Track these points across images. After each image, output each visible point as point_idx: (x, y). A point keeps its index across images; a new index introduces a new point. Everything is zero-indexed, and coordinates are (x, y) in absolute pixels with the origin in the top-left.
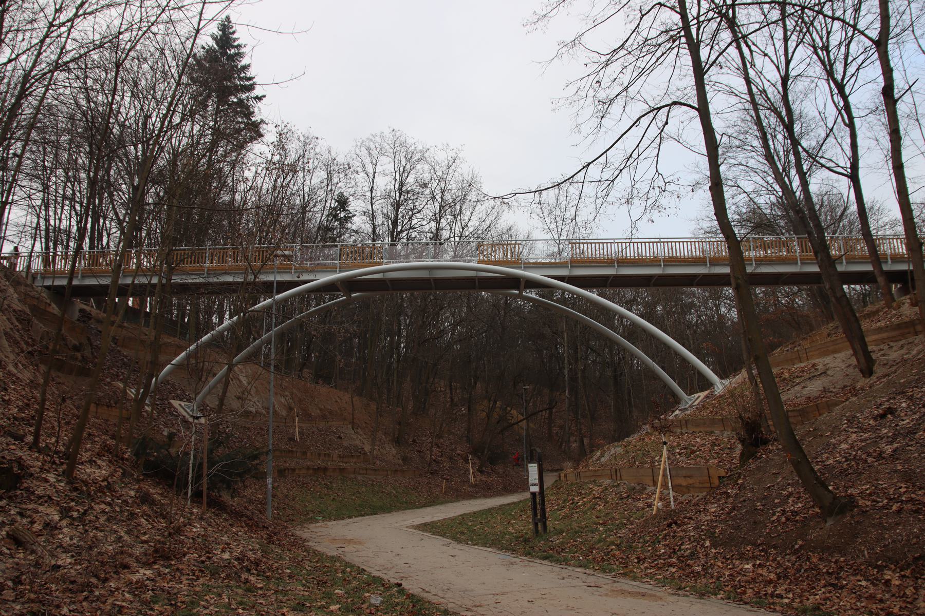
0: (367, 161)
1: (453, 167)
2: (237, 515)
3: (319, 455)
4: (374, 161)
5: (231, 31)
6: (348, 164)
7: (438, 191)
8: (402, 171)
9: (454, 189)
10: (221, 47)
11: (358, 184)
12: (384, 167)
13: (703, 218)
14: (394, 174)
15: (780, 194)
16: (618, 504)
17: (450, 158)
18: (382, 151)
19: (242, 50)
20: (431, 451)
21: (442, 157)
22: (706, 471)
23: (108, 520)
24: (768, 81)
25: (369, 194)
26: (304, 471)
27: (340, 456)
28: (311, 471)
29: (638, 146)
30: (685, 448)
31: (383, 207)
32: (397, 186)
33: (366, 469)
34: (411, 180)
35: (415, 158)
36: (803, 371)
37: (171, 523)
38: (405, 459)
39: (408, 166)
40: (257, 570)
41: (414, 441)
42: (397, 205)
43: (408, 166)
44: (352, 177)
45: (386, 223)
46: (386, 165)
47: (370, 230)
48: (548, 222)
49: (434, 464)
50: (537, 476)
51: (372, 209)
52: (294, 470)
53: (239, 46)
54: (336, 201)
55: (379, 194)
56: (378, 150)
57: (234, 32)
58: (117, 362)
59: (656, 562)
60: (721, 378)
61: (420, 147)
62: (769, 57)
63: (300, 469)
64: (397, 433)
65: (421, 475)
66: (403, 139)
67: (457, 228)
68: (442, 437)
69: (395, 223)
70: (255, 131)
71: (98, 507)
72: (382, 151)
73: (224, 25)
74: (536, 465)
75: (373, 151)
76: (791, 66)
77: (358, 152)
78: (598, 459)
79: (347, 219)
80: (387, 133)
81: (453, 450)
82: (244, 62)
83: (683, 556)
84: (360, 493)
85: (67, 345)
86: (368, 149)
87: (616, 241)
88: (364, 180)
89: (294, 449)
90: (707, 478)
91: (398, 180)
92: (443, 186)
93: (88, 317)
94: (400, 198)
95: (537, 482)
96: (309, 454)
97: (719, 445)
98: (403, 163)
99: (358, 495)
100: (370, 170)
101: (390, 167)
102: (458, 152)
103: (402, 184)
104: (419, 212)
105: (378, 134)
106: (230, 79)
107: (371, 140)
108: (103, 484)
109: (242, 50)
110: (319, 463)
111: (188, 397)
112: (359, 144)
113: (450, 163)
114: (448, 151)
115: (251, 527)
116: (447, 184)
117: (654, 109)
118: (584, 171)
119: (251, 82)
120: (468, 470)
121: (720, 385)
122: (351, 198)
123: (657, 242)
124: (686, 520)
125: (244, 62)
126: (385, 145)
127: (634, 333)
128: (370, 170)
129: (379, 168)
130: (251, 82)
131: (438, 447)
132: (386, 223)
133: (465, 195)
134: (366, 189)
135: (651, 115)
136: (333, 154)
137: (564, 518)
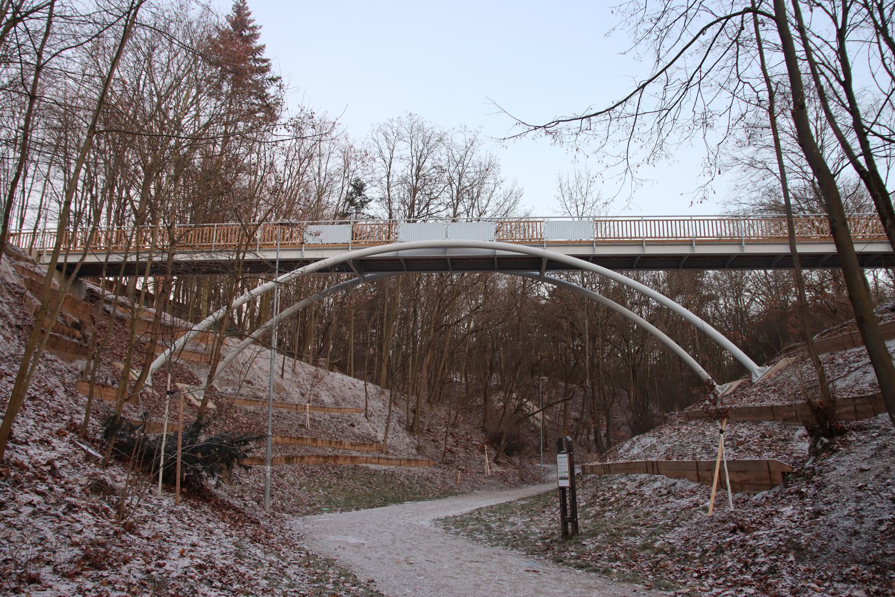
0: (384, 146)
1: (471, 149)
2: (220, 506)
3: (330, 442)
4: (391, 147)
5: (246, 12)
6: (366, 151)
7: (456, 176)
8: (419, 156)
9: (471, 173)
10: (235, 29)
11: (375, 171)
12: (401, 153)
13: (731, 200)
14: (411, 159)
15: (811, 176)
16: (657, 501)
17: (467, 140)
18: (399, 137)
19: (258, 32)
20: (446, 440)
21: (460, 140)
22: (766, 466)
23: (34, 514)
24: (818, 37)
25: (386, 179)
26: (314, 459)
27: (352, 445)
28: (321, 459)
29: (700, 66)
30: (730, 440)
31: (399, 193)
32: (414, 170)
33: (379, 458)
34: (428, 164)
35: (432, 142)
36: (861, 355)
37: (123, 518)
38: (418, 448)
39: (425, 151)
40: (220, 581)
41: (428, 430)
42: (414, 190)
43: (425, 151)
44: (370, 164)
45: (403, 208)
46: (403, 149)
47: (387, 215)
48: (569, 206)
49: (448, 454)
50: (567, 469)
51: (389, 195)
52: (302, 458)
53: (254, 28)
54: (354, 186)
55: (395, 179)
56: (395, 135)
57: (249, 14)
58: (122, 342)
59: (722, 579)
60: (759, 365)
61: (437, 131)
62: (823, 7)
63: (309, 457)
64: (411, 421)
65: (435, 465)
66: (420, 123)
67: (474, 212)
68: (457, 427)
69: (411, 208)
70: (270, 112)
71: (24, 498)
72: (399, 137)
73: (238, 6)
74: (566, 455)
75: (391, 138)
76: (850, 15)
77: (375, 137)
78: (628, 450)
79: (363, 203)
80: (404, 117)
81: (468, 440)
82: (259, 43)
83: (760, 572)
84: (371, 483)
85: (65, 322)
86: (385, 134)
87: (644, 218)
88: (380, 165)
89: (305, 436)
90: (767, 474)
91: (415, 166)
92: (461, 169)
93: (96, 297)
94: (416, 183)
95: (567, 475)
96: (319, 441)
97: (770, 436)
98: (421, 147)
99: (369, 485)
100: (387, 155)
101: (408, 153)
102: (476, 134)
103: (419, 169)
104: (436, 198)
105: (395, 119)
106: (245, 60)
107: (388, 125)
108: (45, 469)
109: (258, 32)
110: (329, 451)
111: (195, 381)
112: (376, 129)
113: (469, 145)
114: (466, 132)
115: (236, 522)
116: (465, 167)
117: (721, 19)
118: (638, 94)
119: (266, 64)
120: (484, 460)
121: (758, 372)
122: (368, 185)
123: (688, 220)
124: (754, 525)
125: (259, 43)
126: (402, 130)
127: (662, 316)
128: (387, 155)
129: (396, 154)
130: (266, 64)
131: (454, 437)
132: (403, 208)
133: (483, 178)
134: (384, 174)
135: (720, 24)
136: (350, 141)
137: (595, 516)
